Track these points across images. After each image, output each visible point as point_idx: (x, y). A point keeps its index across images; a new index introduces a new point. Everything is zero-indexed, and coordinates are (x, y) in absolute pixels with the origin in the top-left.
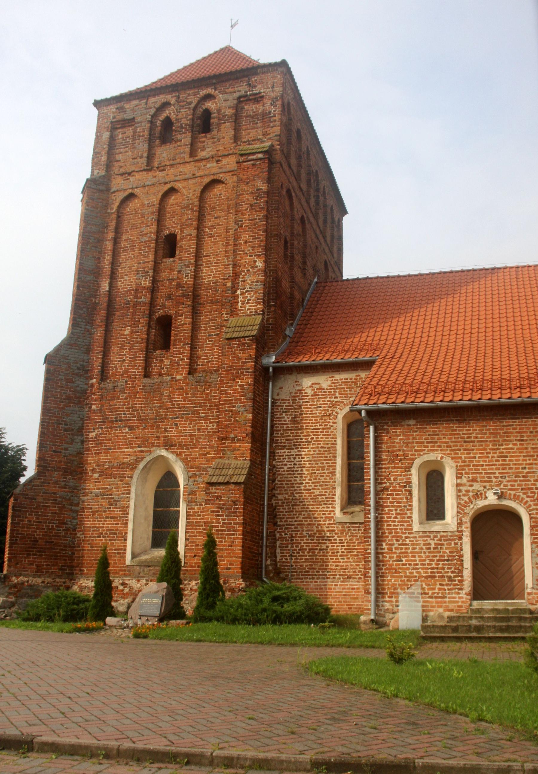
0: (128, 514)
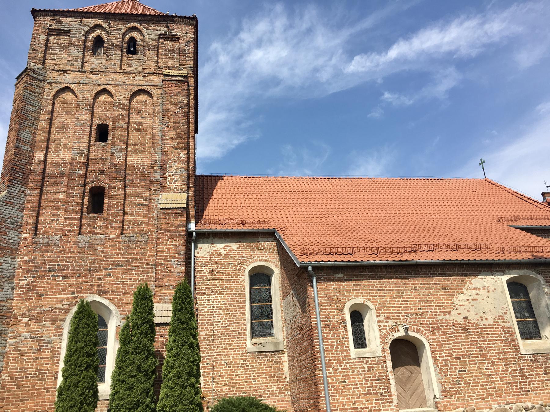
0: (59, 354)
